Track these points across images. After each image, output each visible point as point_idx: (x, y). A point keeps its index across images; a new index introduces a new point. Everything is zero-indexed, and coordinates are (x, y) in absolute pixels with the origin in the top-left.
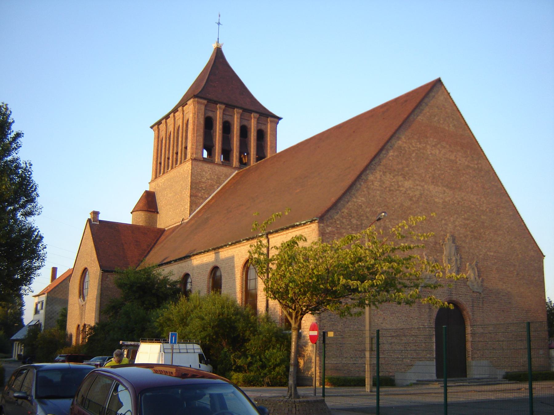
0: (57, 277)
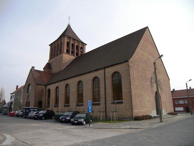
0: (18, 88)
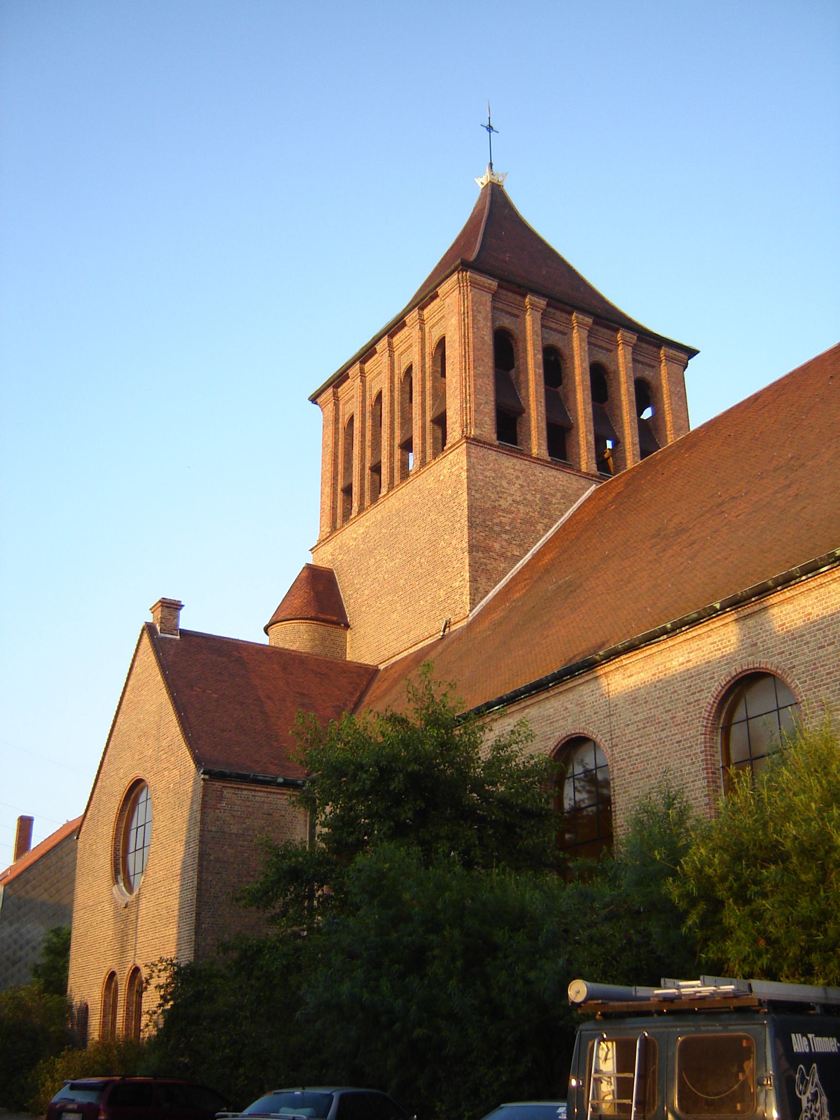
0: (33, 845)
